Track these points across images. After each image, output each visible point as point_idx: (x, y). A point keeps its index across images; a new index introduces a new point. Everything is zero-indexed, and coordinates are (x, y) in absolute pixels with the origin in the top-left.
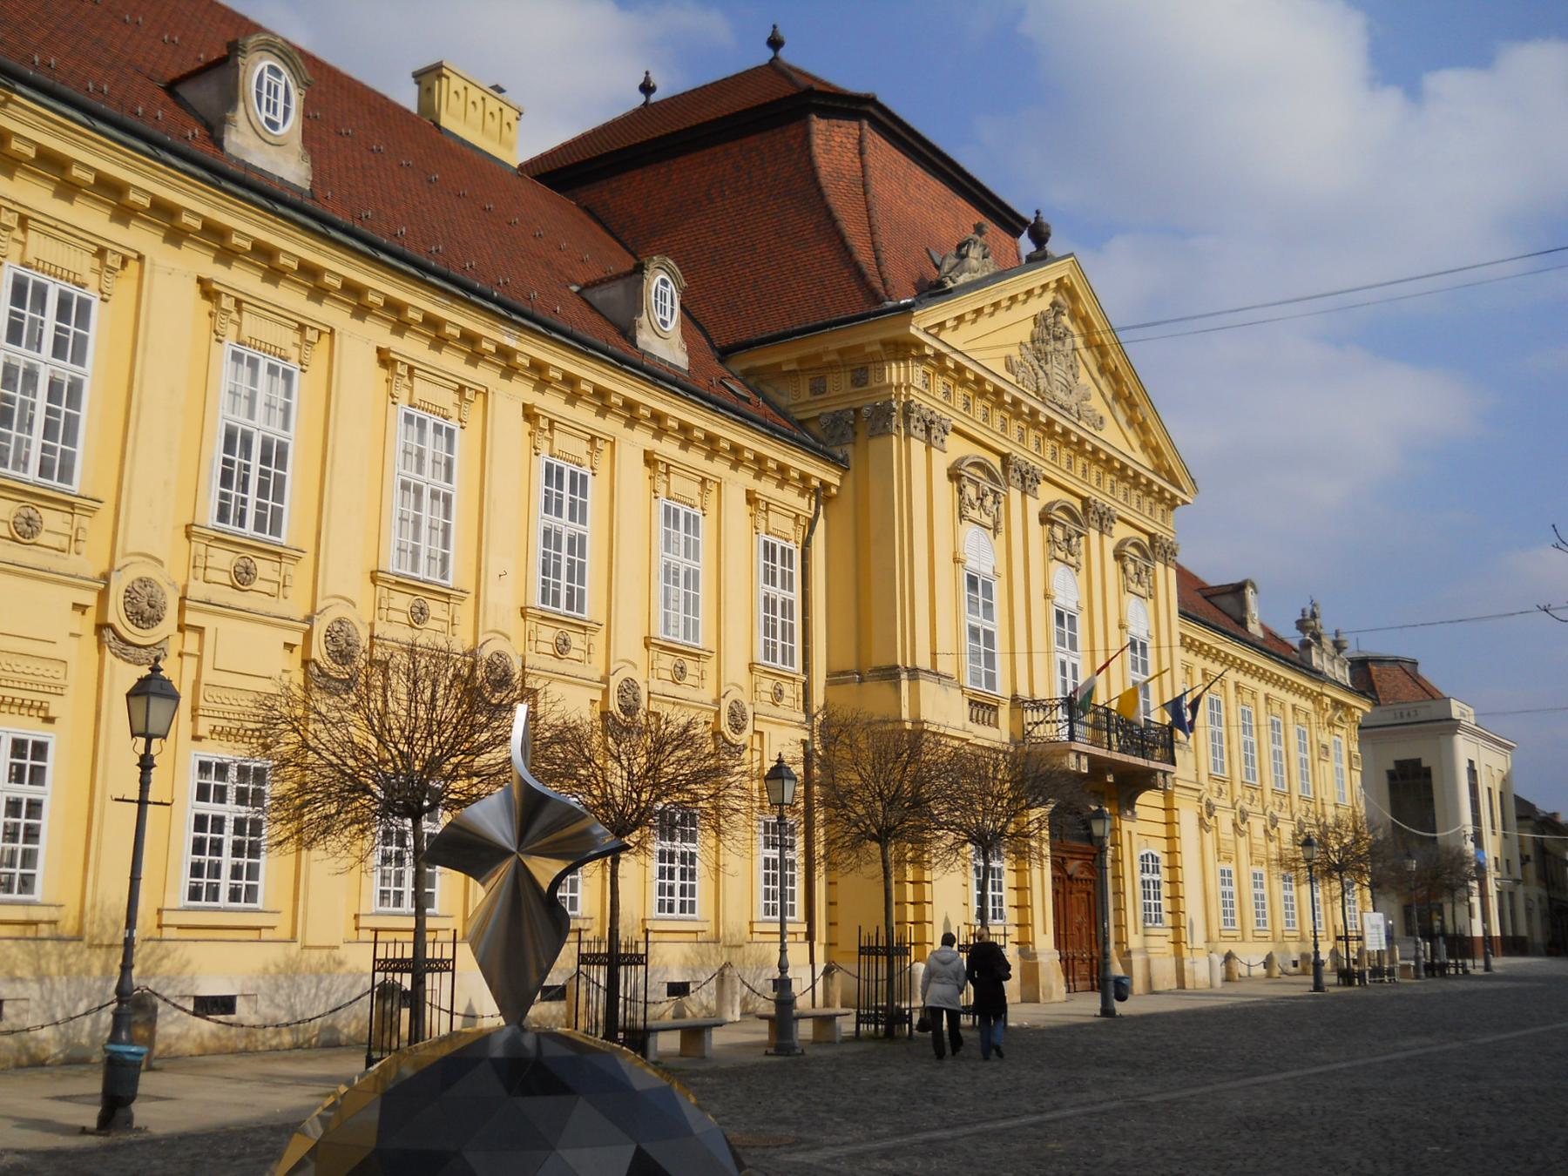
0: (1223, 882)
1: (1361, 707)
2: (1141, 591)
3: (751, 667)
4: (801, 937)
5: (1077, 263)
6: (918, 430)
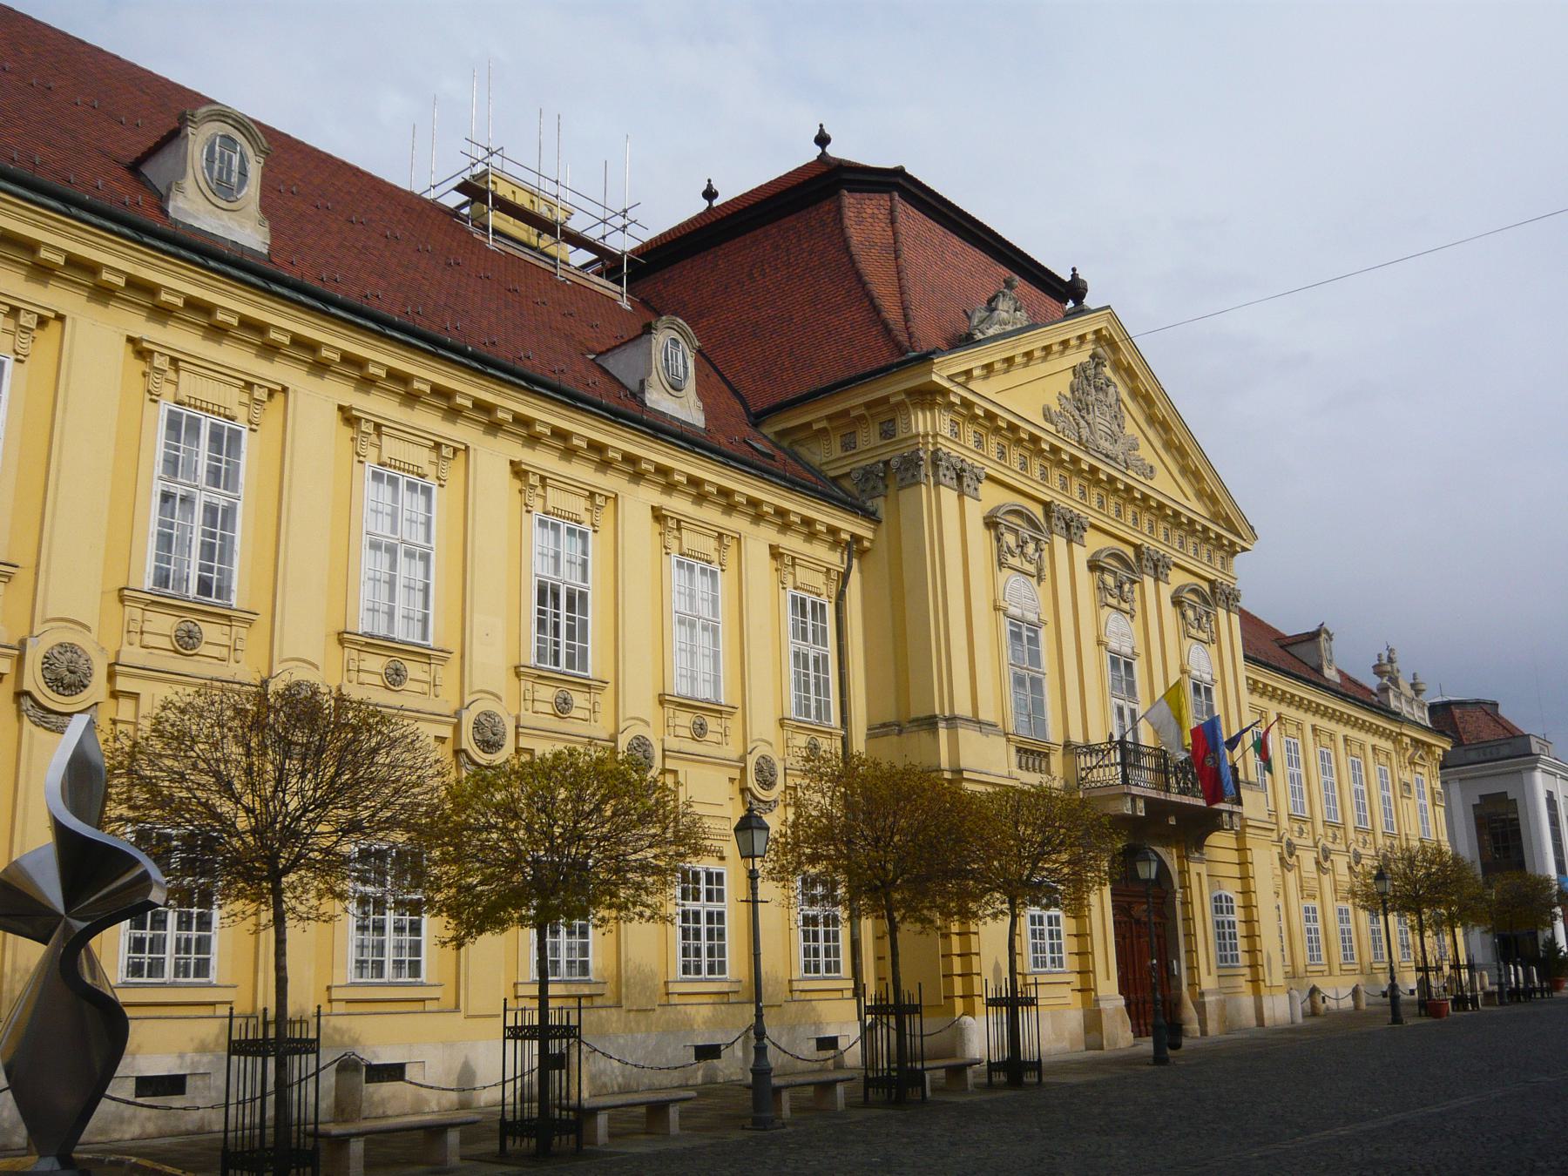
0: (1308, 919)
1: (1442, 745)
2: (1204, 636)
3: (782, 722)
4: (849, 994)
5: (1113, 315)
6: (948, 477)
